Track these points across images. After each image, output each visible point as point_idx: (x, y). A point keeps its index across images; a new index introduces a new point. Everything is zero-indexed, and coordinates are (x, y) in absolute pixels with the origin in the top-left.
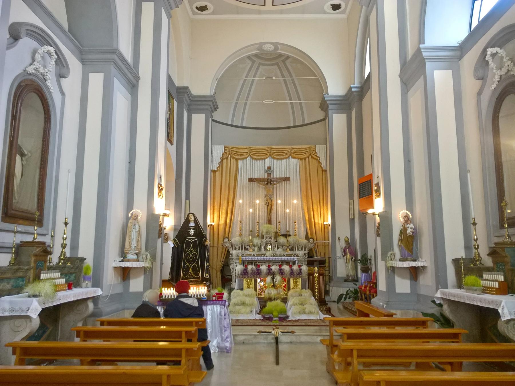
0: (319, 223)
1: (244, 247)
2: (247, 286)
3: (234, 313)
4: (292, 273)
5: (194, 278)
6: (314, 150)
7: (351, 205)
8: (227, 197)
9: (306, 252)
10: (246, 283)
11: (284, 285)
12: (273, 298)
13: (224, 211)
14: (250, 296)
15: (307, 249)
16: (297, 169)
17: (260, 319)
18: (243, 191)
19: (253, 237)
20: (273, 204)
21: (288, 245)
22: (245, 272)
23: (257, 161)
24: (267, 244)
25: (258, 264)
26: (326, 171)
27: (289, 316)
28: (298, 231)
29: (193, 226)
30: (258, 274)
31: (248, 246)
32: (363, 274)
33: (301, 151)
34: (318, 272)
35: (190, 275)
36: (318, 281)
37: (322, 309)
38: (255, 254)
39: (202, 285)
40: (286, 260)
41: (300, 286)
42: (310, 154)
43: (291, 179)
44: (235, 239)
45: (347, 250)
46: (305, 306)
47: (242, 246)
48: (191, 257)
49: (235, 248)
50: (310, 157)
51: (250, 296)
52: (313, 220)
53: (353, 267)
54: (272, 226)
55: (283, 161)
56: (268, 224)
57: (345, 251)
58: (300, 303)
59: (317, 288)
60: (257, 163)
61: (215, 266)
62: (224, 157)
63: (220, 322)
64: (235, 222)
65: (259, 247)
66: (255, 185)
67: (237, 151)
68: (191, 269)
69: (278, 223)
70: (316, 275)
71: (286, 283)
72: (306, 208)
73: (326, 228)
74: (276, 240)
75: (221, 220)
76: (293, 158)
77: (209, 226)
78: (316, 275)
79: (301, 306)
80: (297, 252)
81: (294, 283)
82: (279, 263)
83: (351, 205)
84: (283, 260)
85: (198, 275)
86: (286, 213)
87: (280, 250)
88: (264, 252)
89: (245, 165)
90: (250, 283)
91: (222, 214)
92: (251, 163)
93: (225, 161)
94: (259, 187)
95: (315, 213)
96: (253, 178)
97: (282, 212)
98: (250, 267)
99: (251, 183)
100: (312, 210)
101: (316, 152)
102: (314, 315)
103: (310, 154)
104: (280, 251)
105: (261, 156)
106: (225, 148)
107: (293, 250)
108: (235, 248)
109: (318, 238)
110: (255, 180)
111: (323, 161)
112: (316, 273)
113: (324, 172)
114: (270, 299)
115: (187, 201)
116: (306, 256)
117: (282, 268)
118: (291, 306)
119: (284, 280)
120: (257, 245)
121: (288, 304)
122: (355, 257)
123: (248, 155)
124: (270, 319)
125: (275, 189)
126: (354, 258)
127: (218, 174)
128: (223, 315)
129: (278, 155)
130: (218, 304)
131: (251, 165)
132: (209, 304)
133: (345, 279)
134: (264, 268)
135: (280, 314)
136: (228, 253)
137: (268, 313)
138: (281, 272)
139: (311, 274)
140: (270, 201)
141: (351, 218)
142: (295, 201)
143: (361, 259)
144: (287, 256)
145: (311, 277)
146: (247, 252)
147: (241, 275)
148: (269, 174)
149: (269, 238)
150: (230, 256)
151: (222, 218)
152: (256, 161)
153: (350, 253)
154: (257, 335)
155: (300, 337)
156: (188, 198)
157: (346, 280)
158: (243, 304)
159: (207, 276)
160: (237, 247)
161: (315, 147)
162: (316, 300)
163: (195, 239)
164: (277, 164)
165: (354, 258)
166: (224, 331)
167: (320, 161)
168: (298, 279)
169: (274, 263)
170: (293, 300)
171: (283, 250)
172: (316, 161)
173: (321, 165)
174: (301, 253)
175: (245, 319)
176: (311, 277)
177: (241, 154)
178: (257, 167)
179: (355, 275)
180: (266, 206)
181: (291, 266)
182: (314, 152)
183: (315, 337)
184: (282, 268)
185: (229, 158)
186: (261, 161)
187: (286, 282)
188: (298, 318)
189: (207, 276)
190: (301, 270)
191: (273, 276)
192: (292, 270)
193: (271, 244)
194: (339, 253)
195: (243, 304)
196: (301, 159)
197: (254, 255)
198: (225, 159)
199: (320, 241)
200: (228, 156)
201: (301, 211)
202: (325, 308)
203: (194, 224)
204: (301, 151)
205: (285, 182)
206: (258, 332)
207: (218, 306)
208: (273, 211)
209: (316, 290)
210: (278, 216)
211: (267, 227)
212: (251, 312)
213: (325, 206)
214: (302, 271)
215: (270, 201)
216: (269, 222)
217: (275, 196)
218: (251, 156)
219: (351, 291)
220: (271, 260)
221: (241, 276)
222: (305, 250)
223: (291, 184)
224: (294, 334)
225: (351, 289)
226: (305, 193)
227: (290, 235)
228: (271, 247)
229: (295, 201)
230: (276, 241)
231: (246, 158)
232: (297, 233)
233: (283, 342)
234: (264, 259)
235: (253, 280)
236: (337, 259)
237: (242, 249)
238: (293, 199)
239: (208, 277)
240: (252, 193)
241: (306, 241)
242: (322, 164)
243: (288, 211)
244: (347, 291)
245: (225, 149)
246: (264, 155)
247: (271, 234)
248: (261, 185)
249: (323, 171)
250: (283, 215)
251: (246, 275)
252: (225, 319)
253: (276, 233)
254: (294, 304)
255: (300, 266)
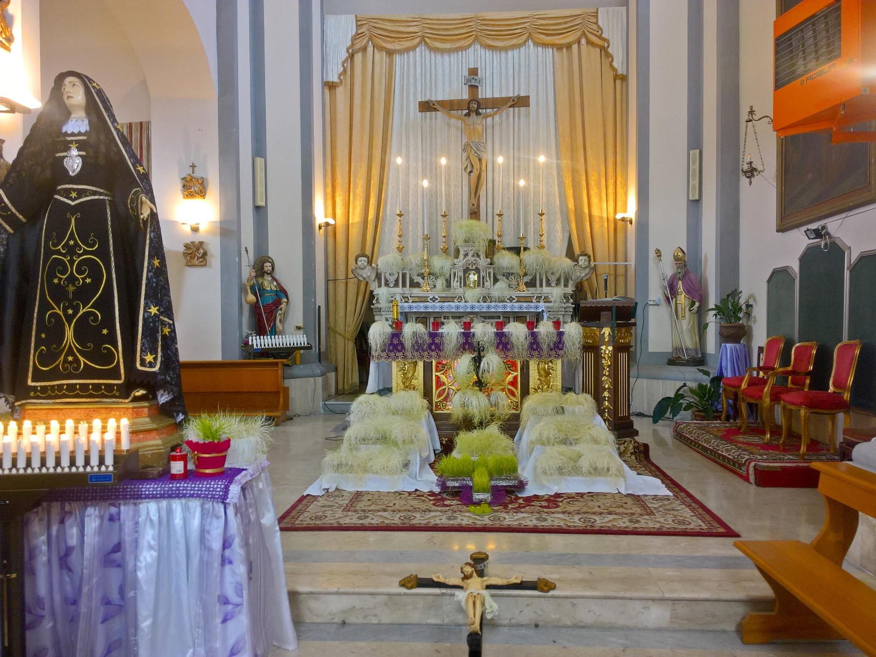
0: (602, 218)
1: (406, 280)
2: (404, 383)
3: (351, 469)
4: (534, 344)
5: (89, 373)
6: (594, 20)
7: (694, 164)
8: (366, 152)
9: (570, 290)
10: (399, 373)
11: (510, 378)
12: (476, 421)
13: (359, 189)
14: (406, 413)
15: (571, 283)
16: (548, 74)
17: (432, 494)
18: (407, 137)
19: (430, 253)
20: (484, 168)
21: (522, 274)
22: (395, 342)
23: (442, 57)
24: (466, 271)
25: (434, 320)
26: (624, 78)
27: (526, 484)
28: (548, 238)
29: (80, 134)
30: (433, 347)
31: (418, 275)
32: (728, 345)
33: (560, 24)
34: (613, 339)
35: (66, 361)
36: (612, 367)
37: (622, 448)
38: (436, 297)
39: (127, 404)
40: (516, 310)
41: (557, 380)
42: (584, 34)
43: (532, 101)
44: (386, 260)
45: (680, 282)
46: (578, 448)
47: (404, 275)
48: (72, 279)
49: (387, 281)
50: (583, 41)
51: (406, 413)
52: (586, 211)
53: (693, 327)
54: (482, 223)
55: (510, 53)
56: (471, 218)
57: (672, 288)
58: (562, 436)
59: (609, 388)
60: (443, 62)
61: (340, 327)
62: (358, 46)
63: (203, 585)
64: (388, 217)
65: (446, 280)
66: (439, 120)
67: (389, 28)
68: (69, 333)
69: (497, 218)
70: (607, 350)
71: (515, 374)
72: (570, 179)
73: (619, 228)
74: (491, 259)
75: (354, 215)
76: (537, 44)
77: (320, 228)
78: (607, 350)
79: (563, 448)
80: (546, 290)
81: (540, 375)
82: (499, 318)
83: (694, 164)
84: (509, 310)
85: (109, 357)
86: (517, 191)
87: (502, 284)
88: (460, 291)
89: (412, 68)
90: (410, 375)
91: (354, 198)
92: (428, 62)
93: (358, 57)
94: (449, 125)
95: (594, 192)
96: (433, 99)
97: (508, 186)
98: (410, 329)
99: (428, 113)
100: (584, 183)
101: (599, 27)
102: (609, 479)
103: (584, 34)
104: (500, 289)
105: (452, 40)
106: (357, 21)
107: (535, 286)
108: (387, 281)
109: (599, 254)
110: (437, 106)
111: (616, 50)
112: (607, 344)
113: (618, 82)
114: (468, 424)
115: (259, 161)
116: (568, 302)
117: (504, 330)
118: (532, 444)
119: (512, 365)
120: (442, 274)
121: (520, 438)
122: (700, 302)
123: (417, 40)
124: (464, 495)
125: (489, 131)
126: (697, 304)
127: (341, 93)
128: (216, 545)
129: (497, 36)
130: (192, 496)
131: (428, 68)
132: (147, 497)
133: (670, 357)
134: (451, 330)
135: (496, 476)
136: (372, 296)
137: (456, 476)
138: (503, 343)
139: (591, 348)
140: (475, 161)
141: (691, 198)
142: (542, 159)
143: (721, 306)
144: (520, 299)
145: (592, 356)
146: (416, 291)
147: (384, 351)
148: (473, 88)
149: (473, 256)
150: (374, 302)
151: (354, 208)
152: (439, 57)
153: (688, 292)
154: (399, 594)
155: (573, 605)
156: (259, 149)
157: (674, 361)
158: (383, 439)
159: (151, 365)
160: (392, 279)
161: (597, 12)
162: (605, 420)
163: (95, 193)
164: (495, 63)
165: (697, 304)
166: (219, 620)
167: (610, 50)
168: (551, 362)
169: (485, 318)
170: (539, 426)
171: (509, 286)
172: (598, 50)
173: (612, 61)
174: (556, 293)
175: (384, 489)
176: (592, 356)
177: (398, 36)
178: (443, 71)
179: (698, 346)
180: (467, 176)
181: (531, 326)
182: (594, 27)
183: (638, 606)
184: (504, 330)
185: (370, 49)
186: (454, 57)
187: (516, 370)
188: (554, 489)
189: (151, 365)
190: (560, 334)
191: (476, 354)
192: (534, 335)
193: (477, 270)
194: (655, 291)
195: (383, 439)
196: (560, 47)
197: (434, 299)
198: (357, 51)
199: (604, 263)
200: (368, 42)
201: (556, 188)
202: (631, 447)
203: (86, 122)
204: (560, 24)
205: (516, 109)
206: (403, 584)
207: (195, 505)
208: (484, 187)
209: (606, 394)
210: (496, 201)
211: (467, 226)
212: (406, 465)
213: (618, 173)
214: (565, 338)
215: (475, 161)
216: (474, 214)
217: (489, 149)
218: (426, 43)
219: (691, 390)
220: (477, 310)
221: (384, 354)
222: (566, 285)
223: (531, 116)
224: (551, 593)
225: (689, 384)
226: (568, 141)
227: (525, 249)
228: (479, 277)
229: (542, 159)
230: (491, 264)
231: (414, 48)
232: (544, 243)
233: (505, 622)
234: (458, 307)
235: (421, 365)
236: (651, 308)
237: (404, 285)
238: (536, 153)
239: (156, 369)
240: (431, 141)
241: (568, 262)
242: (615, 60)
243: (522, 183)
244: (679, 390)
245: (359, 23)
246: (460, 39)
247: (477, 244)
248: (453, 121)
249: (616, 77)
250: (509, 198)
251: (399, 351)
252: (225, 561)
253: (492, 242)
254: (544, 442)
255: (557, 324)
